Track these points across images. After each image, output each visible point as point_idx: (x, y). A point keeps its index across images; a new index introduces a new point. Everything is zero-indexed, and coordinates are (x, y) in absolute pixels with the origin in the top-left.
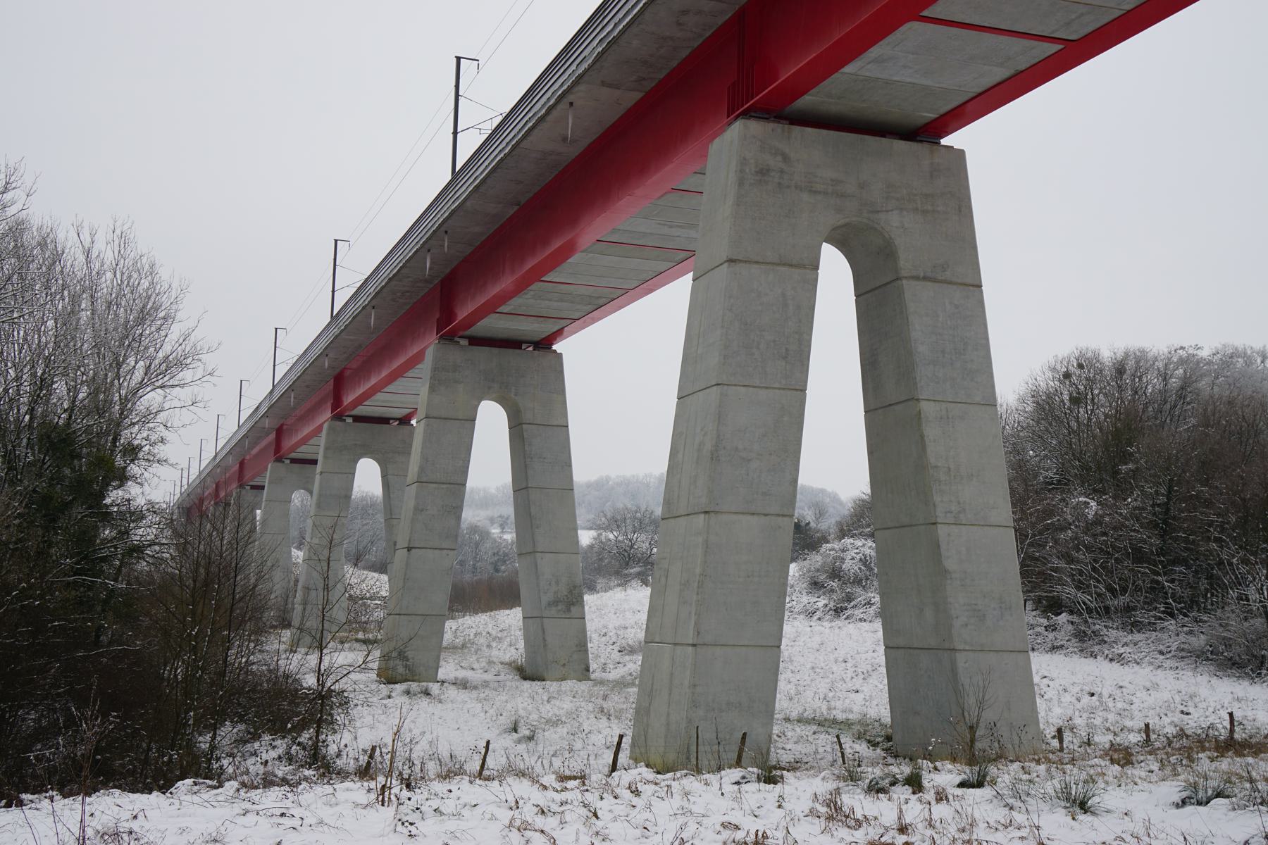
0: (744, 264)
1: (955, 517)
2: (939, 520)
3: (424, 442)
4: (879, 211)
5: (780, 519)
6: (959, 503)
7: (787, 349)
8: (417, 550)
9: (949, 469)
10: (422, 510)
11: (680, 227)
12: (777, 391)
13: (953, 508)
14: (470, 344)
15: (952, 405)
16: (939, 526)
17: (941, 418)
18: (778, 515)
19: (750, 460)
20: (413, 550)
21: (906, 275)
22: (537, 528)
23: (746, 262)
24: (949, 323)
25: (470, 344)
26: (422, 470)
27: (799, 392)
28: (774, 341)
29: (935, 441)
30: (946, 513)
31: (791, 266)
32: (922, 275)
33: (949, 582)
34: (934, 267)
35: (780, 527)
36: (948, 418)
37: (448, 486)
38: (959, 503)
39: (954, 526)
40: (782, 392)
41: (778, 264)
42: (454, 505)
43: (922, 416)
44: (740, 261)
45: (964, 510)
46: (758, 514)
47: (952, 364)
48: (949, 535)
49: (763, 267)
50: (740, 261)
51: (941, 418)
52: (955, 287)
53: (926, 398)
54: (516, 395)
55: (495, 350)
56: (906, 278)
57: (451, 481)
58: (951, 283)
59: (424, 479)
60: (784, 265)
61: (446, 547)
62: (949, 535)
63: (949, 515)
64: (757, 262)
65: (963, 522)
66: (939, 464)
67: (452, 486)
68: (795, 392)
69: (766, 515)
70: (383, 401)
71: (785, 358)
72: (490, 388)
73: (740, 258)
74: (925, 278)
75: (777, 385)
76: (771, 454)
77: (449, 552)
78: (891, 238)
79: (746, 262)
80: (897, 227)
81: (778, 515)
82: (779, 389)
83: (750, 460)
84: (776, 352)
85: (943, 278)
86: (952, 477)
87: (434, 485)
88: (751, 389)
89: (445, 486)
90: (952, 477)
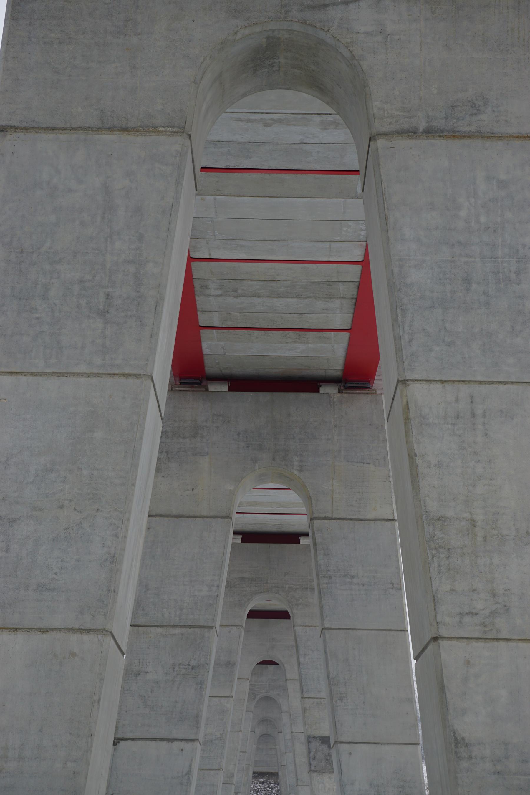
0: (21, 135)
1: (484, 625)
2: (443, 632)
3: (231, 560)
4: (326, 6)
5: (75, 638)
6: (494, 594)
7: (108, 296)
8: (129, 742)
9: (473, 523)
10: (138, 674)
11: (280, 121)
12: (82, 380)
13: (479, 606)
14: (231, 389)
15: (484, 388)
16: (443, 643)
17: (458, 417)
18: (73, 630)
19: (14, 521)
20: (122, 743)
21: (386, 129)
22: (341, 699)
23: (27, 129)
24: (483, 219)
25: (230, 389)
26: (138, 604)
27: (131, 381)
28: (82, 281)
29: (439, 466)
30: (462, 614)
31: (126, 130)
32: (423, 125)
33: (464, 764)
34: (453, 107)
35: (73, 655)
36: (473, 415)
37: (184, 630)
38: (494, 594)
39: (481, 644)
40: (94, 381)
41: (98, 130)
42: (193, 663)
43: (412, 414)
44: (15, 129)
45: (507, 609)
46: (28, 630)
47: (487, 304)
48: (468, 663)
49: (63, 136)
50: (15, 129)
51: (458, 417)
52: (500, 144)
53: (424, 376)
54: (301, 471)
55: (264, 397)
56: (385, 134)
57: (189, 623)
58: (492, 136)
59: (142, 621)
60: (111, 129)
61: (180, 736)
62: (468, 663)
63: (467, 619)
64: (52, 129)
65: (504, 635)
66: (450, 513)
67: (190, 630)
68: (122, 380)
69: (44, 631)
70: (250, 504)
71: (103, 313)
72: (255, 460)
73: (17, 124)
74: (429, 132)
75: (83, 368)
76: (62, 507)
77: (182, 745)
78: (353, 57)
79: (27, 129)
80: (367, 33)
81: (73, 630)
82: (89, 375)
83: (14, 521)
84: (83, 302)
85: (473, 128)
86: (479, 539)
87: (159, 630)
88: (24, 379)
89: (177, 631)
90: (479, 539)
